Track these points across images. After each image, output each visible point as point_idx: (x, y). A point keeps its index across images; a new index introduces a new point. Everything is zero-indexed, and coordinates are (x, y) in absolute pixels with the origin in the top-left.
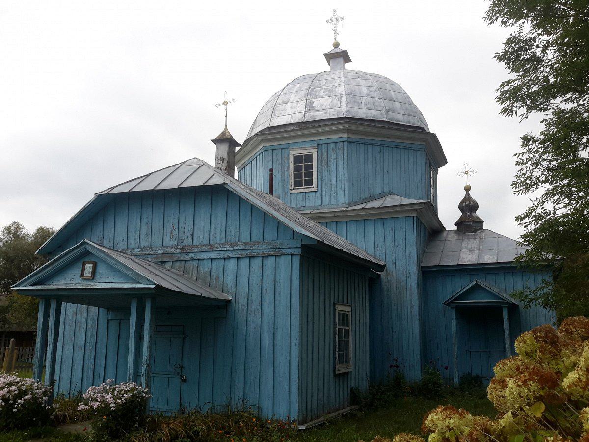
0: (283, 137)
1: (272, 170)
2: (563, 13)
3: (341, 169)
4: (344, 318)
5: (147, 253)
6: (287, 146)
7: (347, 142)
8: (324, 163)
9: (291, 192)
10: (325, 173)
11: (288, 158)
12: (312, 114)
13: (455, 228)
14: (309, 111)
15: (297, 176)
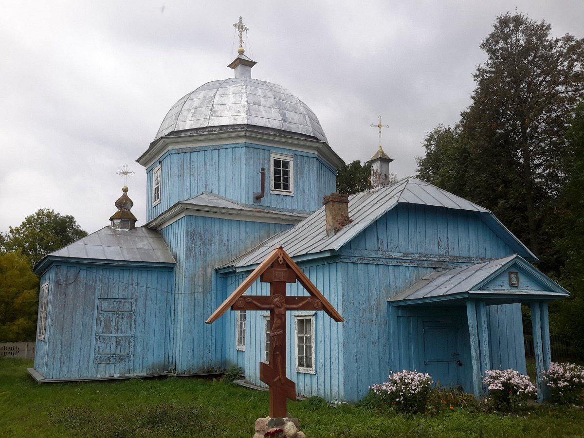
0: (279, 141)
2: (574, 116)
3: (312, 181)
5: (425, 259)
6: (268, 148)
7: (317, 159)
8: (299, 173)
10: (300, 182)
15: (277, 179)
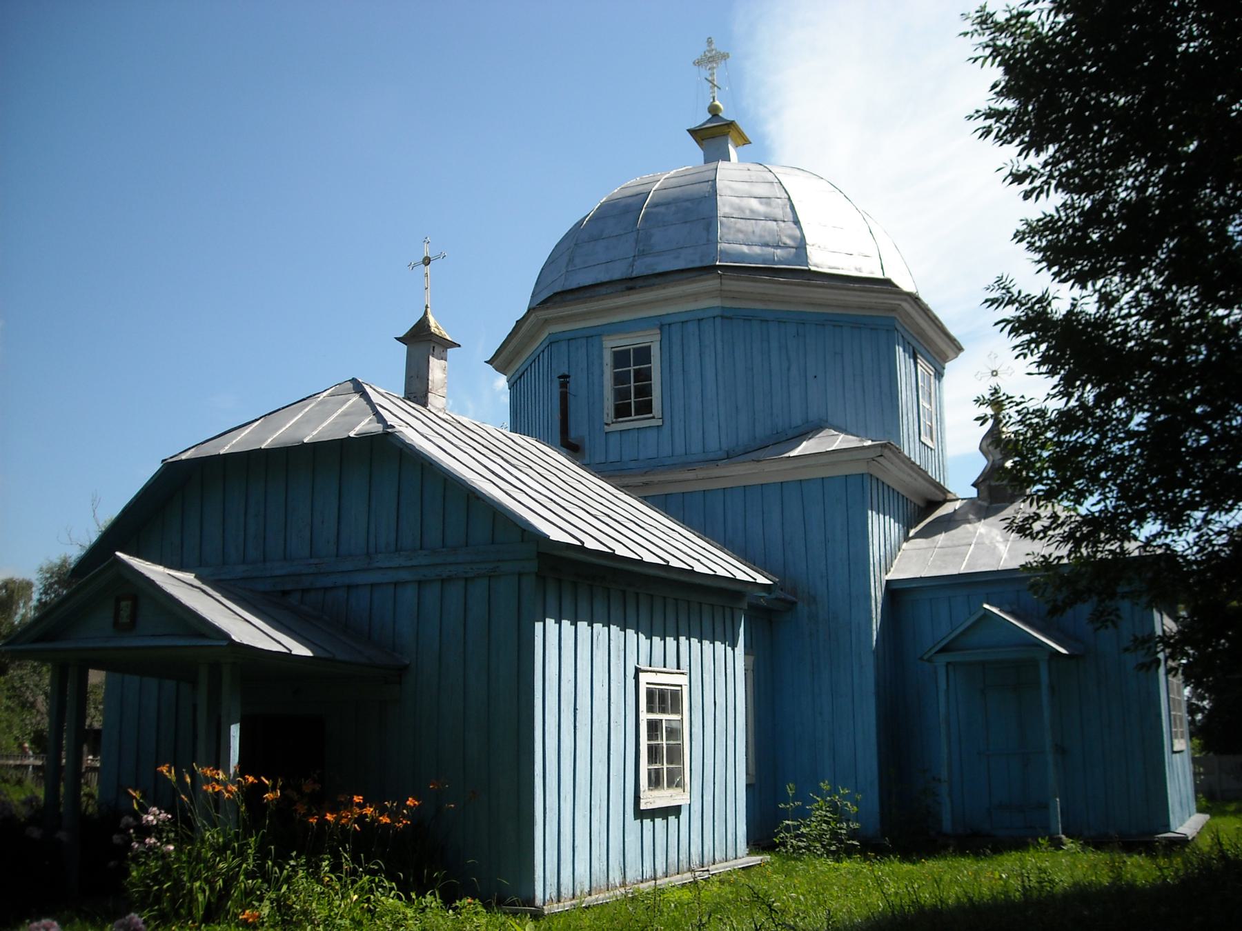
1: (564, 380)
4: (663, 699)
7: (722, 317)
9: (607, 429)
11: (601, 357)
12: (648, 260)
13: (973, 493)
14: (642, 254)
15: (621, 395)
